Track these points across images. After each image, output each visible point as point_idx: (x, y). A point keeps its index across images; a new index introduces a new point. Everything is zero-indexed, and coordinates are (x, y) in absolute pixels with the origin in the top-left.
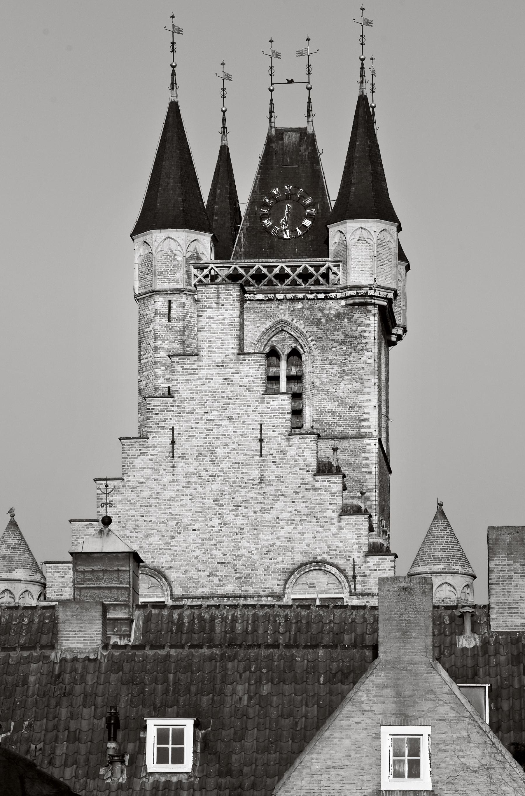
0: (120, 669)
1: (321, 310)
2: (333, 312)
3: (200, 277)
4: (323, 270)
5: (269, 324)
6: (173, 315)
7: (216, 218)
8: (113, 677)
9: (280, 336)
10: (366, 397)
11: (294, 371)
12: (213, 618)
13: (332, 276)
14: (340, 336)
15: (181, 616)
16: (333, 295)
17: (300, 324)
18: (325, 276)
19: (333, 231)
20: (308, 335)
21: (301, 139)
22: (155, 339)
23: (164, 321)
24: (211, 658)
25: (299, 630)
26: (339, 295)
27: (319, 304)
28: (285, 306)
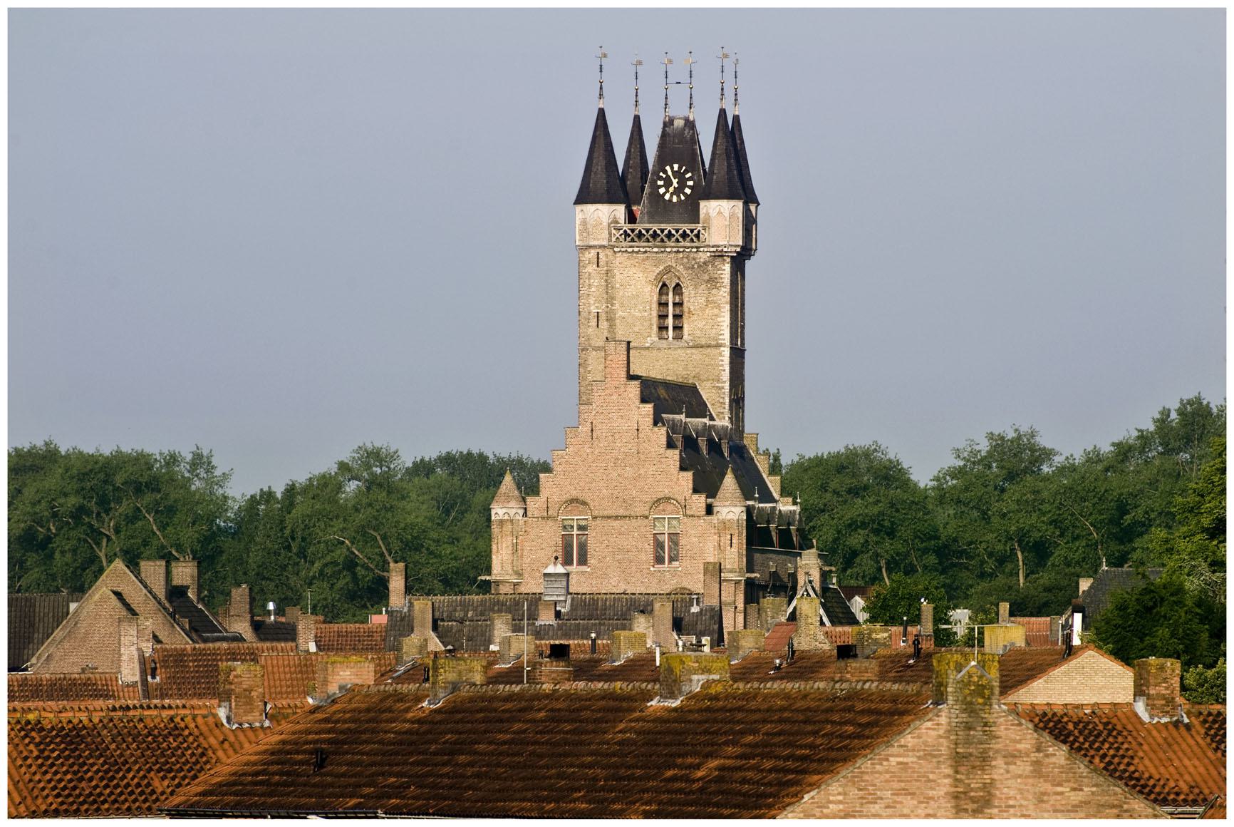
0: (562, 629)
1: (694, 259)
2: (702, 260)
3: (618, 235)
4: (695, 232)
5: (661, 268)
6: (600, 263)
7: (631, 170)
8: (559, 633)
9: (669, 275)
10: (722, 319)
11: (677, 300)
12: (598, 599)
13: (701, 236)
14: (706, 277)
15: (585, 598)
16: (702, 249)
17: (681, 268)
18: (698, 236)
19: (703, 204)
20: (686, 276)
21: (685, 125)
22: (589, 279)
23: (595, 266)
24: (595, 624)
25: (631, 605)
26: (706, 250)
27: (692, 255)
28: (672, 255)
